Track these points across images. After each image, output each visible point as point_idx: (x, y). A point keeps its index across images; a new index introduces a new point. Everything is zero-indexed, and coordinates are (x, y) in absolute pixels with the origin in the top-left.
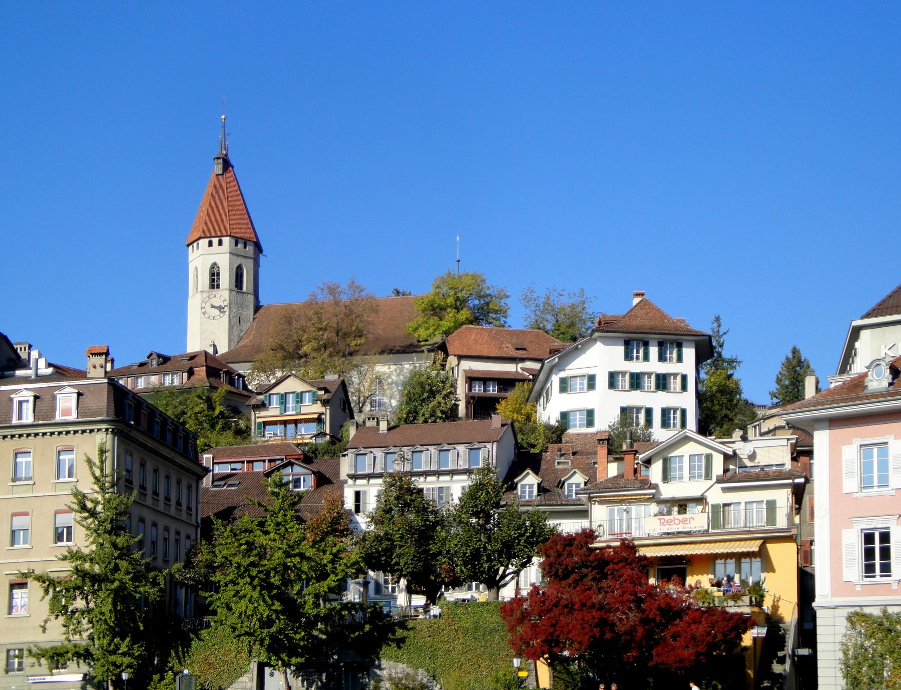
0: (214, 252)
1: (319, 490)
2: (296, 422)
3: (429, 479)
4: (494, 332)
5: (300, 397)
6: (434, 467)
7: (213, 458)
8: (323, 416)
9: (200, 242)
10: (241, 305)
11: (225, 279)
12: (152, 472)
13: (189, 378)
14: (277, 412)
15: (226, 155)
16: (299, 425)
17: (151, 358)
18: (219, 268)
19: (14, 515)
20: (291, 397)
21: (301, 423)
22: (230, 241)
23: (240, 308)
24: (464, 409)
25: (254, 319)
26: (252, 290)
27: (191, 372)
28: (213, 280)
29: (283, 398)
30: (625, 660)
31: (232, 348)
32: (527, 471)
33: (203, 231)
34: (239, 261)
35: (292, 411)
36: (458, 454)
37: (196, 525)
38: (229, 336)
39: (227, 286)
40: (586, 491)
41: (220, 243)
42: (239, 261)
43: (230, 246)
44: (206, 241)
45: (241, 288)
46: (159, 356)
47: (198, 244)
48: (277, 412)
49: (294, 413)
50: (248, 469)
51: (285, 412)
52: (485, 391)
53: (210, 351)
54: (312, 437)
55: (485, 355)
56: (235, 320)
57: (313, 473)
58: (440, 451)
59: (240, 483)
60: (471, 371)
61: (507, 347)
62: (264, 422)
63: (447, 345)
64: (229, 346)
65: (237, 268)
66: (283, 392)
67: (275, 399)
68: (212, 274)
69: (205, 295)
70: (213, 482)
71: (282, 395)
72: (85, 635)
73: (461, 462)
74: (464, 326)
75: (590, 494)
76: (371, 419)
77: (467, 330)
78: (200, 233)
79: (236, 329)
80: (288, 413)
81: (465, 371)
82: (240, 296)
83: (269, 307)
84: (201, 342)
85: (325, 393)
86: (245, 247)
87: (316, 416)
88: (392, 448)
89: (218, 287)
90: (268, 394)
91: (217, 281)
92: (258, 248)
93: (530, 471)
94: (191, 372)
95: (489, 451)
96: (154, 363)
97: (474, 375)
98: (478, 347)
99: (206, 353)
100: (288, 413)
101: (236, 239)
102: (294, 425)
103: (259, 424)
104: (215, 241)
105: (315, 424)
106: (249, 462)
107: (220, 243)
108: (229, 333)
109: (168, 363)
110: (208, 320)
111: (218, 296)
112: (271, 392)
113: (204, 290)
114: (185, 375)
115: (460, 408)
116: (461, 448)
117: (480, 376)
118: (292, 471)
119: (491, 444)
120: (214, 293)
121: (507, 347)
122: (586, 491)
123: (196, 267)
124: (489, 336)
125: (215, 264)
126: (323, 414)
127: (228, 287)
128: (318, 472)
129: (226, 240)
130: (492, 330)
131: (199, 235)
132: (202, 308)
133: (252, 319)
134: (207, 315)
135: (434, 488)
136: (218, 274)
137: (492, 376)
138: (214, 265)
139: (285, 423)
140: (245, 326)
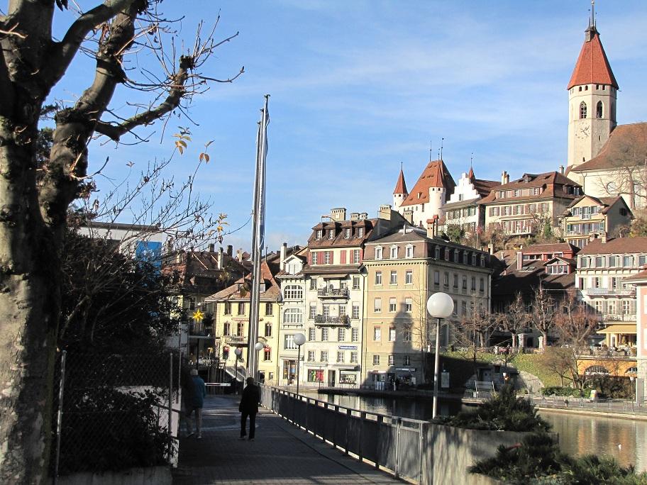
3: (619, 272)
11: (589, 113)
12: (450, 285)
27: (545, 187)
30: (469, 382)
31: (594, 157)
33: (576, 81)
38: (592, 148)
41: (587, 88)
44: (578, 87)
45: (601, 116)
46: (529, 176)
64: (592, 156)
79: (597, 144)
84: (575, 154)
86: (604, 89)
92: (614, 86)
99: (557, 173)
104: (583, 87)
107: (587, 88)
109: (535, 181)
112: (575, 206)
114: (541, 189)
129: (590, 86)
136: (586, 109)
138: (583, 103)
140: (604, 141)
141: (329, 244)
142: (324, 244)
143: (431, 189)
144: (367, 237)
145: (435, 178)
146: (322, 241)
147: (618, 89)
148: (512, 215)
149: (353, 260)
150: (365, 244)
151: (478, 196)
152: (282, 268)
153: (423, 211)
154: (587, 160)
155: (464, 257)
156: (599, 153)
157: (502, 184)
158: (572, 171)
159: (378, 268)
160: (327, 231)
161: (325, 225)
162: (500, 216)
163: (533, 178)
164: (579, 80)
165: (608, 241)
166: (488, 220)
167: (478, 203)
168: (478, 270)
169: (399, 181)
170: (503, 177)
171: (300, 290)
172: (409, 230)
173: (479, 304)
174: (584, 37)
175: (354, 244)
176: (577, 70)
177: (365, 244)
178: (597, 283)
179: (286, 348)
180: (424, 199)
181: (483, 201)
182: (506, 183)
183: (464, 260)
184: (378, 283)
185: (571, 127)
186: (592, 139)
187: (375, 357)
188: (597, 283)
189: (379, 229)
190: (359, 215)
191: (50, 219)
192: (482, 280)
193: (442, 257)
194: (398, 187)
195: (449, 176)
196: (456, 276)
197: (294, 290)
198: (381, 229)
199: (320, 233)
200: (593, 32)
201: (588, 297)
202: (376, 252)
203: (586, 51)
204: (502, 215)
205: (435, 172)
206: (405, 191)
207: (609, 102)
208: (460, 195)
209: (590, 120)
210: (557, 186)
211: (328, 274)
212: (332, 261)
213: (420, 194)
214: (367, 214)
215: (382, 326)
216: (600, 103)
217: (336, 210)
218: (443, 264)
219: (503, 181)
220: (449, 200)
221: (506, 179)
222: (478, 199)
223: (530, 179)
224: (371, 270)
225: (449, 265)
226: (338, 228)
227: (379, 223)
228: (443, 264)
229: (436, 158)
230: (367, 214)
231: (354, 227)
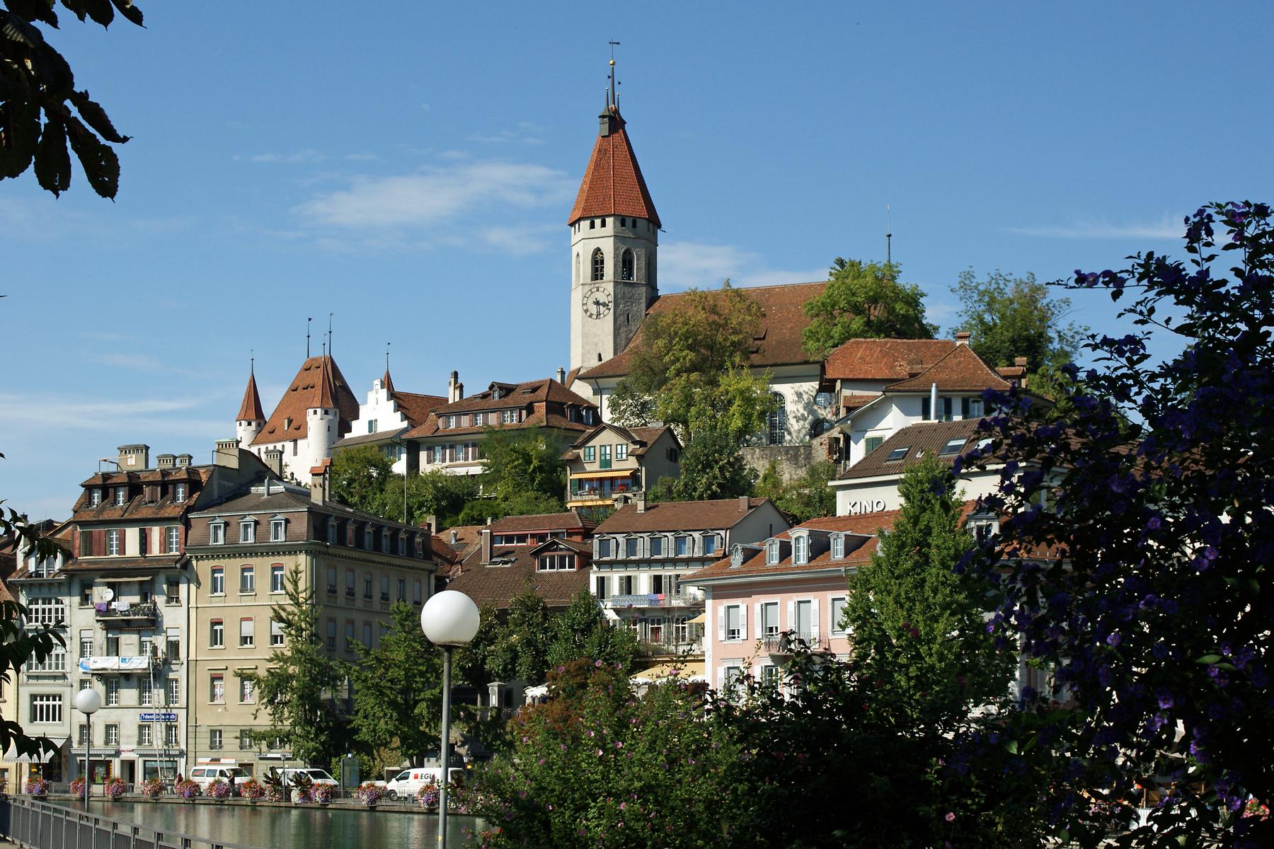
9: (582, 223)
12: (339, 590)
13: (528, 415)
15: (617, 111)
17: (494, 389)
19: (242, 620)
22: (614, 223)
23: (629, 304)
25: (647, 315)
28: (596, 270)
38: (615, 342)
39: (612, 278)
41: (603, 225)
43: (615, 227)
44: (588, 222)
45: (630, 275)
56: (622, 319)
61: (900, 366)
65: (625, 253)
69: (587, 288)
72: (287, 723)
74: (853, 340)
77: (854, 346)
81: (845, 397)
82: (627, 289)
83: (667, 297)
84: (583, 347)
87: (628, 473)
94: (530, 409)
95: (722, 538)
96: (496, 395)
98: (864, 367)
104: (598, 222)
107: (603, 225)
108: (614, 336)
111: (601, 289)
114: (524, 412)
116: (696, 535)
120: (597, 285)
121: (900, 366)
127: (612, 278)
129: (610, 221)
132: (583, 305)
134: (588, 313)
136: (602, 262)
138: (598, 251)
141: (115, 515)
142: (106, 516)
143: (311, 411)
144: (192, 502)
145: (319, 390)
146: (101, 510)
147: (659, 226)
148: (470, 461)
149: (165, 545)
150: (190, 516)
151: (405, 424)
152: (20, 564)
153: (295, 454)
155: (384, 540)
157: (451, 401)
158: (580, 378)
159: (215, 563)
160: (111, 490)
161: (106, 476)
163: (507, 390)
164: (590, 214)
165: (647, 509)
166: (425, 467)
167: (405, 436)
168: (411, 563)
169: (248, 393)
170: (452, 388)
171: (60, 606)
172: (280, 488)
174: (598, 129)
175: (167, 515)
177: (190, 516)
178: (628, 585)
179: (34, 697)
180: (297, 431)
181: (414, 434)
182: (457, 399)
183: (400, 547)
184: (216, 590)
185: (577, 296)
187: (213, 733)
188: (628, 585)
189: (215, 487)
190: (175, 458)
193: (341, 541)
194: (246, 407)
195: (345, 388)
196: (402, 581)
197: (47, 607)
198: (219, 484)
199: (97, 496)
200: (615, 122)
202: (212, 530)
203: (601, 152)
204: (451, 460)
205: (317, 378)
206: (259, 414)
208: (370, 423)
209: (612, 284)
210: (554, 408)
211: (118, 576)
212: (122, 549)
213: (290, 422)
214: (190, 457)
215: (225, 674)
217: (125, 450)
218: (344, 553)
219: (452, 396)
220: (349, 430)
221: (457, 392)
222: (405, 431)
223: (503, 393)
224: (203, 568)
225: (355, 554)
226: (134, 485)
227: (216, 474)
228: (344, 553)
229: (318, 352)
230: (190, 457)
231: (166, 484)
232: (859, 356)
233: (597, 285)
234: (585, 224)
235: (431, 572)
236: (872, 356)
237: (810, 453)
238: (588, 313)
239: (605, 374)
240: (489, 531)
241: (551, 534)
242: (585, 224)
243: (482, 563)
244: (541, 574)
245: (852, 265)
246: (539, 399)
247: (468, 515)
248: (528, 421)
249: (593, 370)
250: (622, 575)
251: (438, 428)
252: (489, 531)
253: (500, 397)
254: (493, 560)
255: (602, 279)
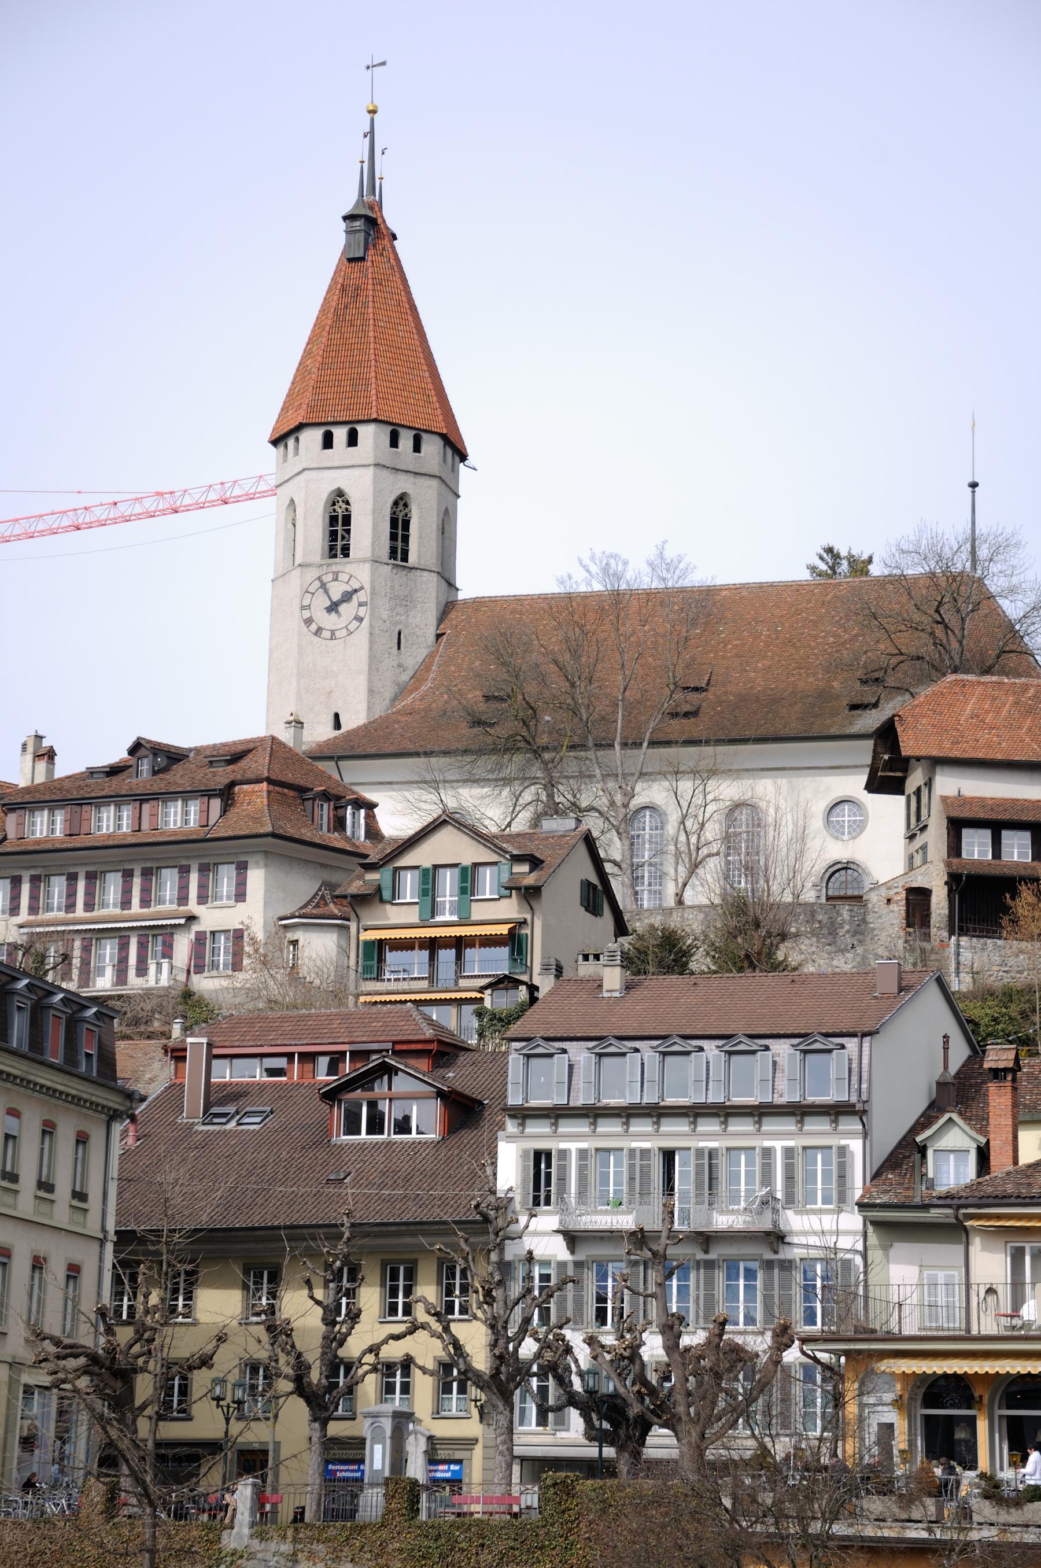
0: (337, 464)
1: (454, 1140)
2: (459, 944)
4: (1032, 691)
5: (468, 877)
6: (715, 1097)
7: (210, 1045)
8: (526, 931)
10: (404, 601)
13: (224, 811)
14: (412, 915)
16: (469, 953)
18: (348, 503)
20: (448, 881)
21: (472, 945)
22: (376, 436)
24: (945, 904)
25: (439, 636)
26: (434, 560)
28: (333, 535)
29: (429, 878)
32: (947, 1116)
33: (311, 408)
34: (329, 483)
35: (451, 914)
36: (775, 1063)
37: (101, 1236)
40: (949, 1201)
41: (353, 440)
42: (404, 484)
43: (376, 447)
47: (297, 440)
48: (412, 915)
49: (455, 918)
50: (301, 1076)
51: (433, 917)
52: (997, 853)
53: (286, 736)
54: (485, 988)
55: (999, 756)
57: (440, 1094)
58: (730, 1053)
59: (272, 1112)
60: (961, 800)
62: (381, 942)
63: (899, 729)
65: (396, 503)
66: (427, 864)
67: (409, 882)
68: (333, 520)
69: (312, 574)
70: (207, 1107)
71: (425, 872)
73: (782, 1084)
74: (951, 678)
75: (959, 1207)
76: (591, 957)
78: (302, 412)
80: (439, 919)
81: (944, 799)
82: (401, 576)
83: (478, 604)
85: (531, 872)
86: (417, 448)
87: (504, 930)
88: (613, 1041)
89: (346, 551)
90: (390, 867)
91: (343, 538)
93: (955, 1116)
97: (966, 814)
100: (439, 919)
101: (390, 428)
102: (454, 951)
103: (369, 944)
104: (340, 434)
105: (504, 952)
106: (303, 1056)
107: (353, 440)
110: (316, 639)
113: (308, 560)
114: (216, 804)
115: (934, 899)
117: (982, 815)
118: (390, 1088)
119: (856, 1040)
120: (334, 568)
122: (949, 1201)
123: (292, 501)
124: (1017, 703)
125: (340, 493)
126: (525, 922)
128: (453, 1092)
129: (366, 433)
130: (1025, 688)
131: (300, 420)
132: (303, 608)
133: (431, 638)
135: (716, 1150)
136: (347, 520)
137: (1015, 818)
139: (432, 945)
140: (415, 655)
147: (463, 457)
148: (80, 912)
154: (348, 724)
156: (394, 699)
162: (24, 916)
165: (628, 987)
173: (740, 1365)
176: (312, 365)
186: (372, 643)
191: (711, 1457)
192: (82, 1140)
201: (560, 1241)
204: (33, 909)
207: (434, 504)
216: (401, 502)
232: (968, 712)
233: (334, 568)
234: (312, 437)
235: (114, 1116)
236: (998, 712)
237: (864, 921)
238: (314, 627)
239: (359, 751)
240: (204, 1040)
241: (351, 1052)
242: (312, 437)
243: (183, 1119)
244: (352, 1146)
245: (852, 560)
246: (250, 775)
247: (650, 850)
248: (239, 822)
249: (329, 743)
250: (790, 1143)
251: (5, 838)
252: (204, 1040)
253: (155, 773)
254: (215, 1110)
255: (347, 555)
